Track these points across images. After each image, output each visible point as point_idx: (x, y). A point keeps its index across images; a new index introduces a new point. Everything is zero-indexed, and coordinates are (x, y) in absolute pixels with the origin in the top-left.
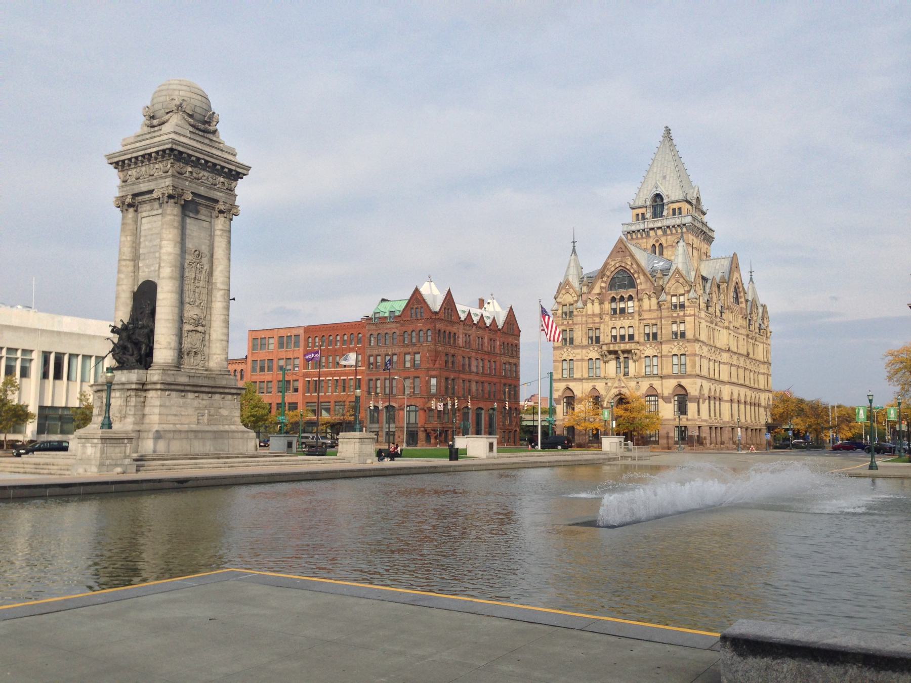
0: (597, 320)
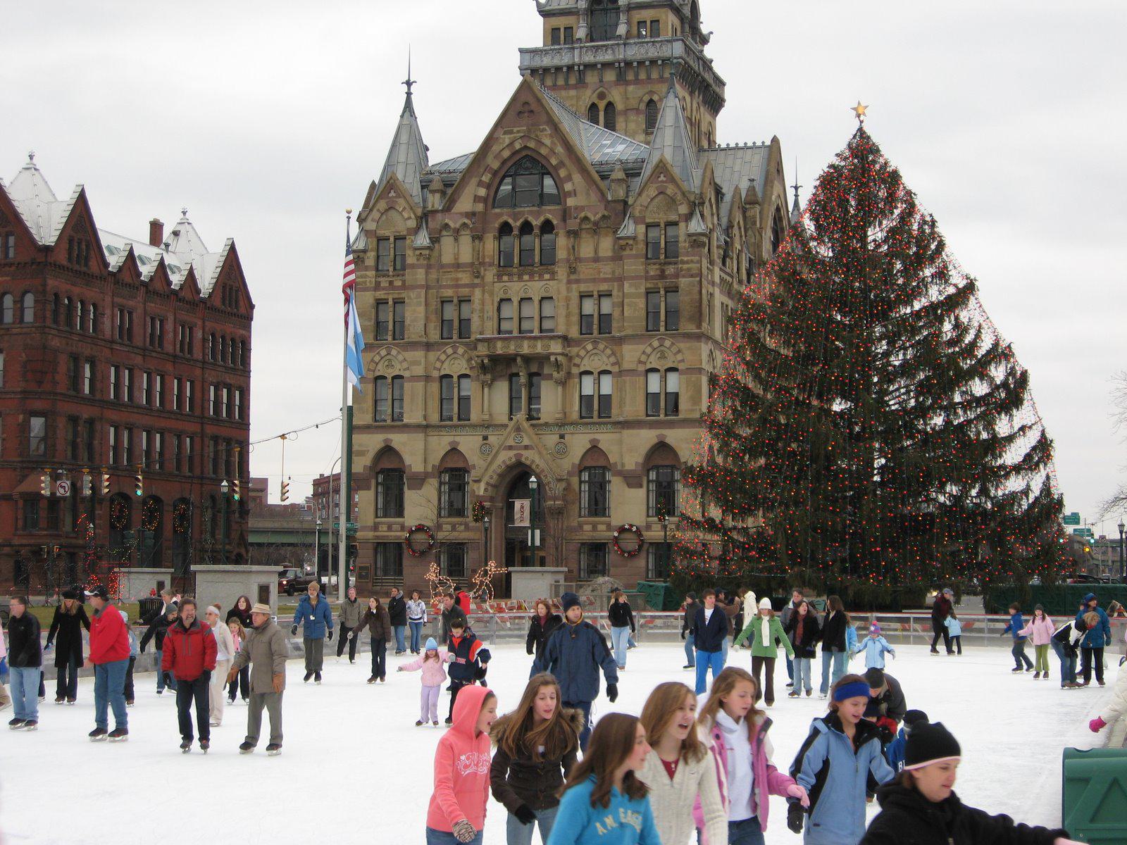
0: (465, 278)
